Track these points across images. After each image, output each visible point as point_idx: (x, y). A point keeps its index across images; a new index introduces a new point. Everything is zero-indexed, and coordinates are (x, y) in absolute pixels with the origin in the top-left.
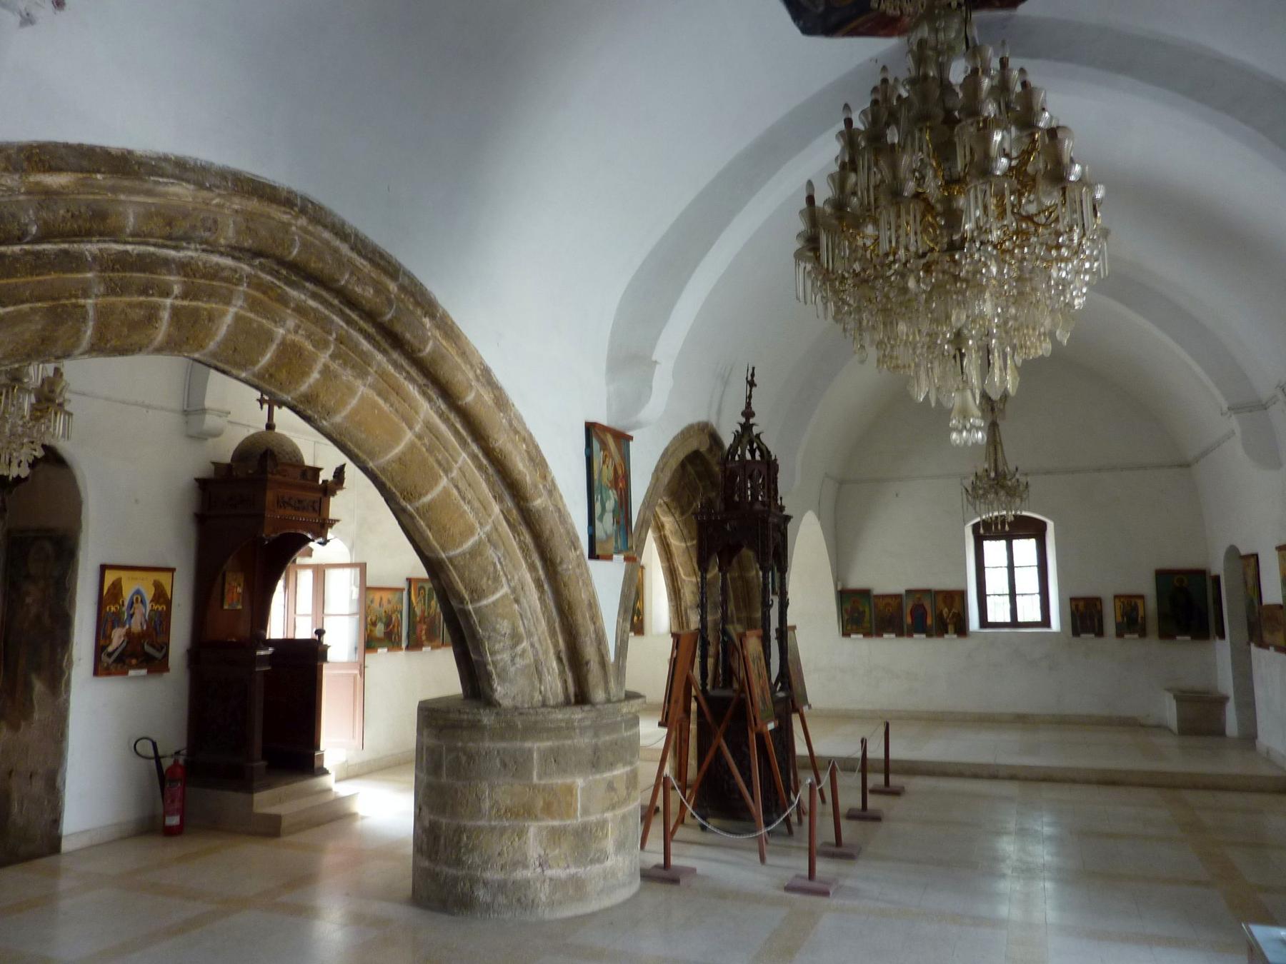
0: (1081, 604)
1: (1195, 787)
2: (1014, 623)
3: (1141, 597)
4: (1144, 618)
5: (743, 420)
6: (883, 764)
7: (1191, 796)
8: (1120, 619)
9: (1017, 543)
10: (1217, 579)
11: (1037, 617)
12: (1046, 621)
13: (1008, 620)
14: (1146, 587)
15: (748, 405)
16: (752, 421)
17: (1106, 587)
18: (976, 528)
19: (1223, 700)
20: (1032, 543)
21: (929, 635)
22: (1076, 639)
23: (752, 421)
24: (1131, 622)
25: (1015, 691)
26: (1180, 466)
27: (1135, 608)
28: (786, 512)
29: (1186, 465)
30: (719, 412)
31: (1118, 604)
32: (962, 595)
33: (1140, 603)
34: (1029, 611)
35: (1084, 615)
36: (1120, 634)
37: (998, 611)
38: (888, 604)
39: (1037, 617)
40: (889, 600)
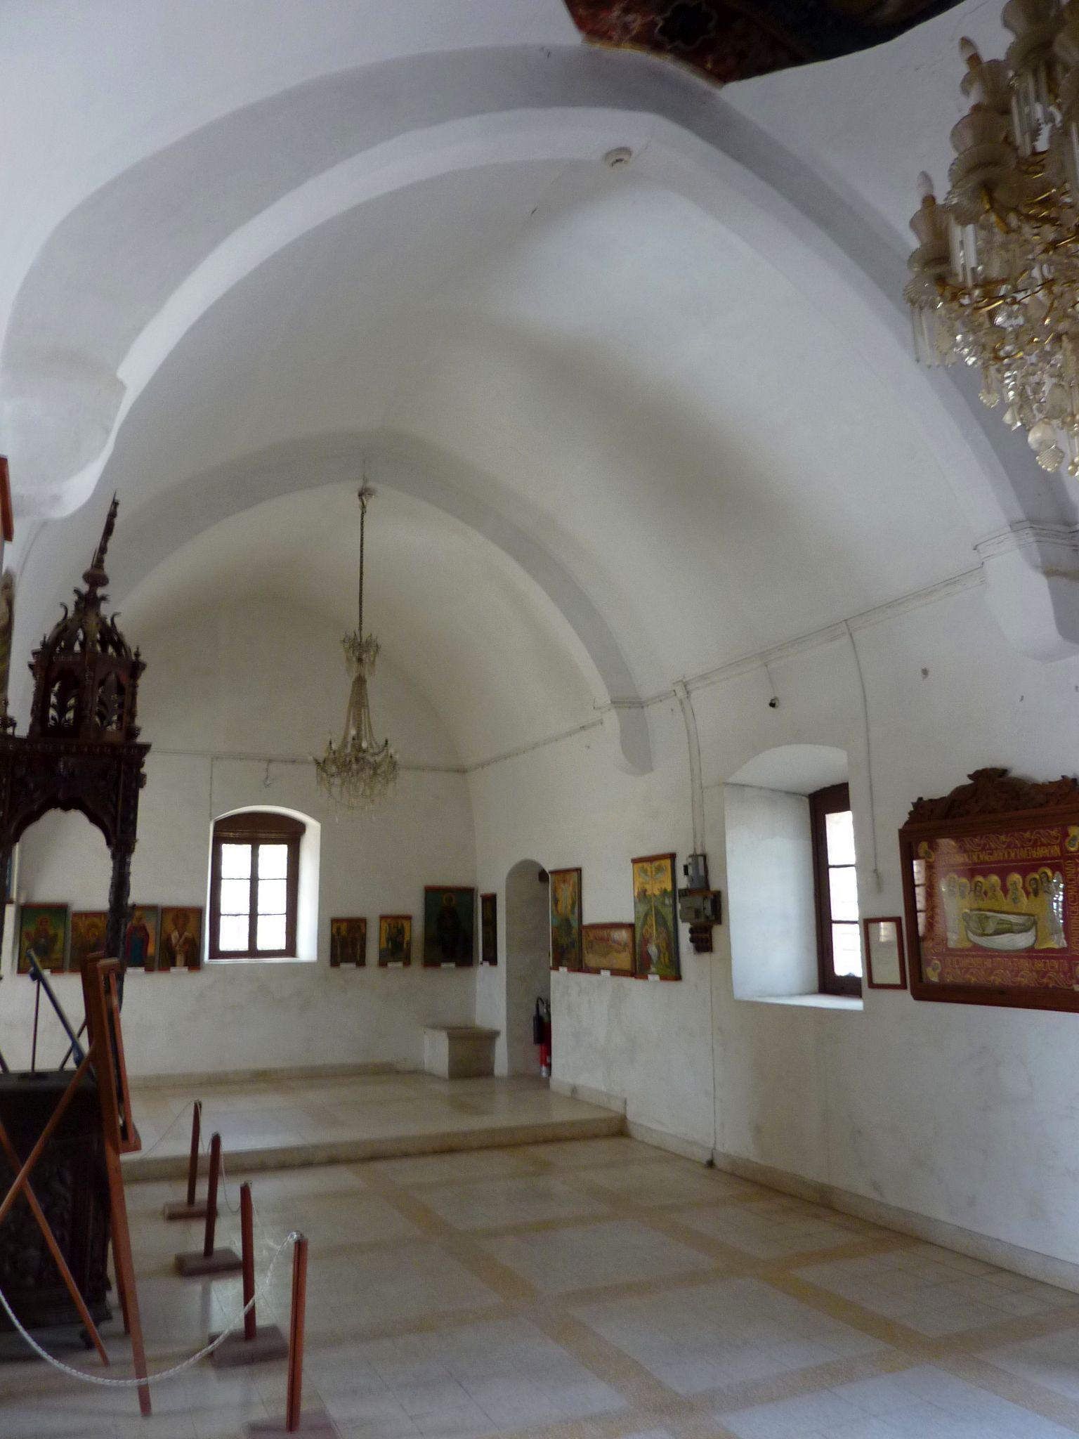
0: (344, 926)
1: (536, 1142)
2: (253, 952)
3: (409, 918)
4: (409, 944)
5: (85, 588)
6: (187, 1165)
7: (380, 1166)
8: (384, 945)
9: (264, 849)
10: (490, 900)
11: (281, 944)
12: (291, 949)
13: (244, 946)
14: (413, 906)
15: (99, 563)
16: (100, 592)
17: (371, 905)
18: (219, 825)
19: (492, 1036)
20: (282, 850)
21: (149, 969)
22: (335, 969)
23: (100, 592)
24: (396, 950)
25: (259, 1041)
26: (458, 771)
27: (401, 932)
28: (141, 739)
29: (462, 771)
30: (23, 568)
31: (385, 925)
32: (199, 912)
33: (406, 924)
34: (272, 936)
35: (345, 941)
36: (383, 964)
37: (233, 936)
38: (93, 926)
39: (281, 944)
40: (96, 920)
